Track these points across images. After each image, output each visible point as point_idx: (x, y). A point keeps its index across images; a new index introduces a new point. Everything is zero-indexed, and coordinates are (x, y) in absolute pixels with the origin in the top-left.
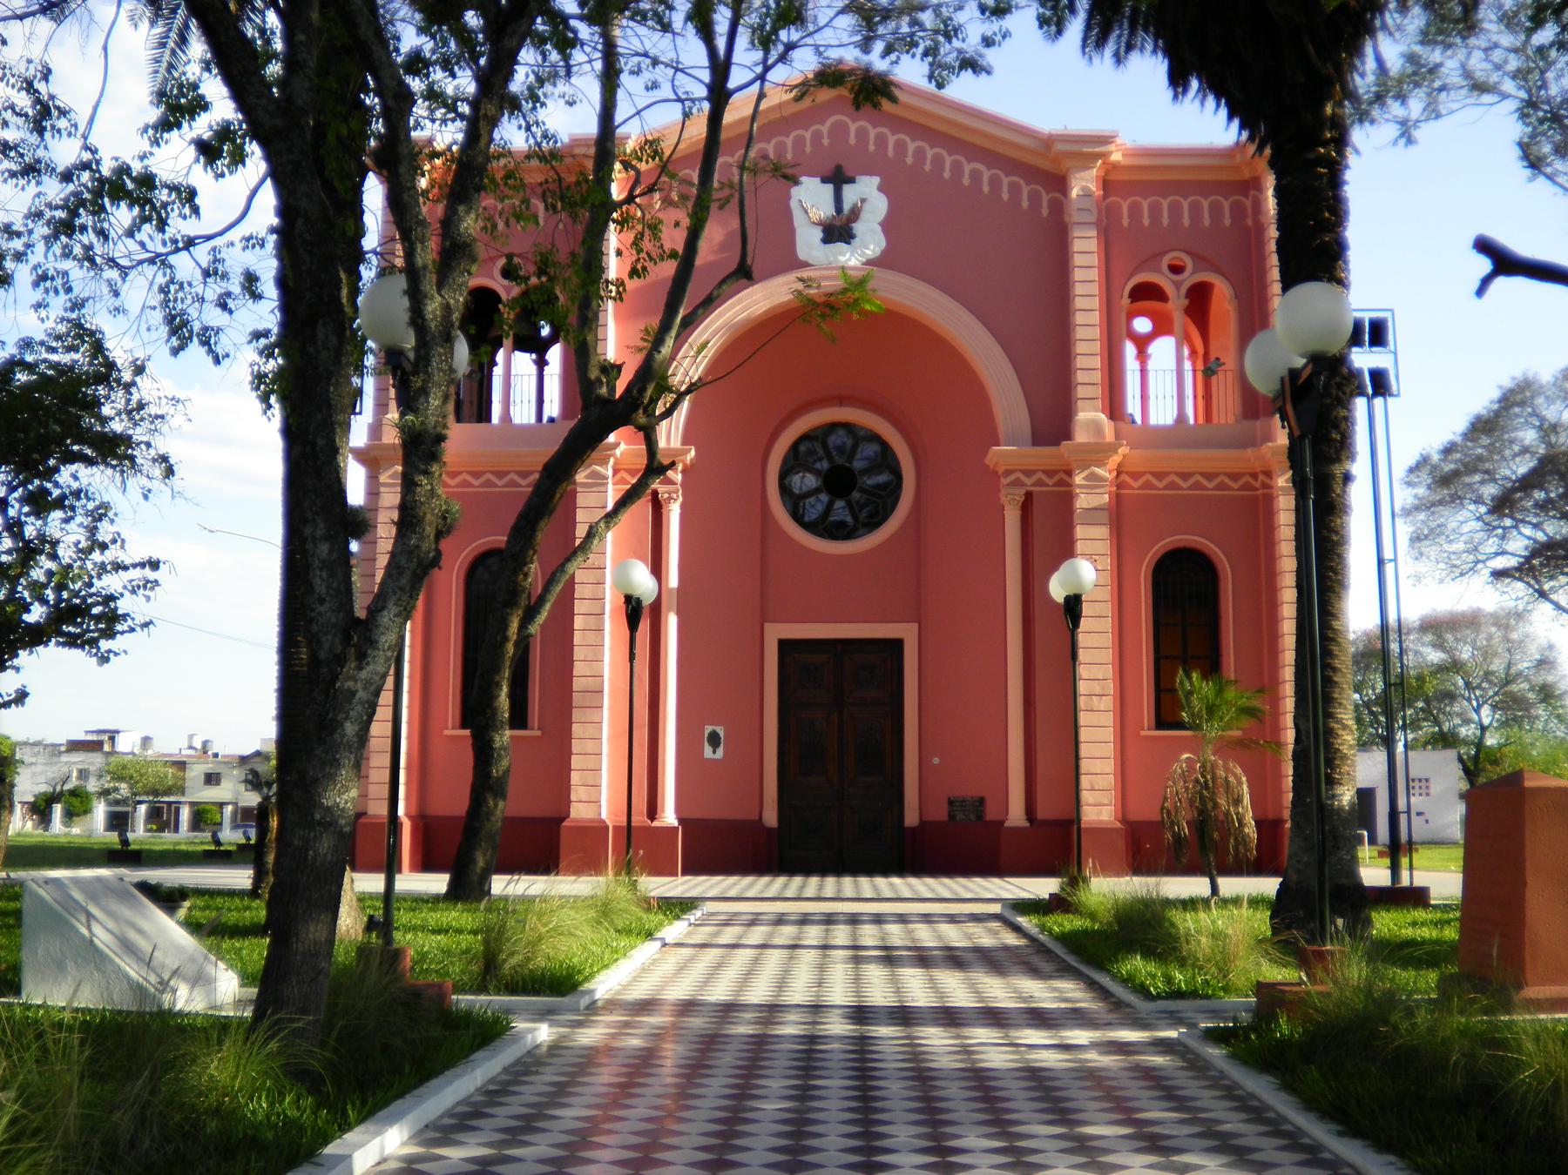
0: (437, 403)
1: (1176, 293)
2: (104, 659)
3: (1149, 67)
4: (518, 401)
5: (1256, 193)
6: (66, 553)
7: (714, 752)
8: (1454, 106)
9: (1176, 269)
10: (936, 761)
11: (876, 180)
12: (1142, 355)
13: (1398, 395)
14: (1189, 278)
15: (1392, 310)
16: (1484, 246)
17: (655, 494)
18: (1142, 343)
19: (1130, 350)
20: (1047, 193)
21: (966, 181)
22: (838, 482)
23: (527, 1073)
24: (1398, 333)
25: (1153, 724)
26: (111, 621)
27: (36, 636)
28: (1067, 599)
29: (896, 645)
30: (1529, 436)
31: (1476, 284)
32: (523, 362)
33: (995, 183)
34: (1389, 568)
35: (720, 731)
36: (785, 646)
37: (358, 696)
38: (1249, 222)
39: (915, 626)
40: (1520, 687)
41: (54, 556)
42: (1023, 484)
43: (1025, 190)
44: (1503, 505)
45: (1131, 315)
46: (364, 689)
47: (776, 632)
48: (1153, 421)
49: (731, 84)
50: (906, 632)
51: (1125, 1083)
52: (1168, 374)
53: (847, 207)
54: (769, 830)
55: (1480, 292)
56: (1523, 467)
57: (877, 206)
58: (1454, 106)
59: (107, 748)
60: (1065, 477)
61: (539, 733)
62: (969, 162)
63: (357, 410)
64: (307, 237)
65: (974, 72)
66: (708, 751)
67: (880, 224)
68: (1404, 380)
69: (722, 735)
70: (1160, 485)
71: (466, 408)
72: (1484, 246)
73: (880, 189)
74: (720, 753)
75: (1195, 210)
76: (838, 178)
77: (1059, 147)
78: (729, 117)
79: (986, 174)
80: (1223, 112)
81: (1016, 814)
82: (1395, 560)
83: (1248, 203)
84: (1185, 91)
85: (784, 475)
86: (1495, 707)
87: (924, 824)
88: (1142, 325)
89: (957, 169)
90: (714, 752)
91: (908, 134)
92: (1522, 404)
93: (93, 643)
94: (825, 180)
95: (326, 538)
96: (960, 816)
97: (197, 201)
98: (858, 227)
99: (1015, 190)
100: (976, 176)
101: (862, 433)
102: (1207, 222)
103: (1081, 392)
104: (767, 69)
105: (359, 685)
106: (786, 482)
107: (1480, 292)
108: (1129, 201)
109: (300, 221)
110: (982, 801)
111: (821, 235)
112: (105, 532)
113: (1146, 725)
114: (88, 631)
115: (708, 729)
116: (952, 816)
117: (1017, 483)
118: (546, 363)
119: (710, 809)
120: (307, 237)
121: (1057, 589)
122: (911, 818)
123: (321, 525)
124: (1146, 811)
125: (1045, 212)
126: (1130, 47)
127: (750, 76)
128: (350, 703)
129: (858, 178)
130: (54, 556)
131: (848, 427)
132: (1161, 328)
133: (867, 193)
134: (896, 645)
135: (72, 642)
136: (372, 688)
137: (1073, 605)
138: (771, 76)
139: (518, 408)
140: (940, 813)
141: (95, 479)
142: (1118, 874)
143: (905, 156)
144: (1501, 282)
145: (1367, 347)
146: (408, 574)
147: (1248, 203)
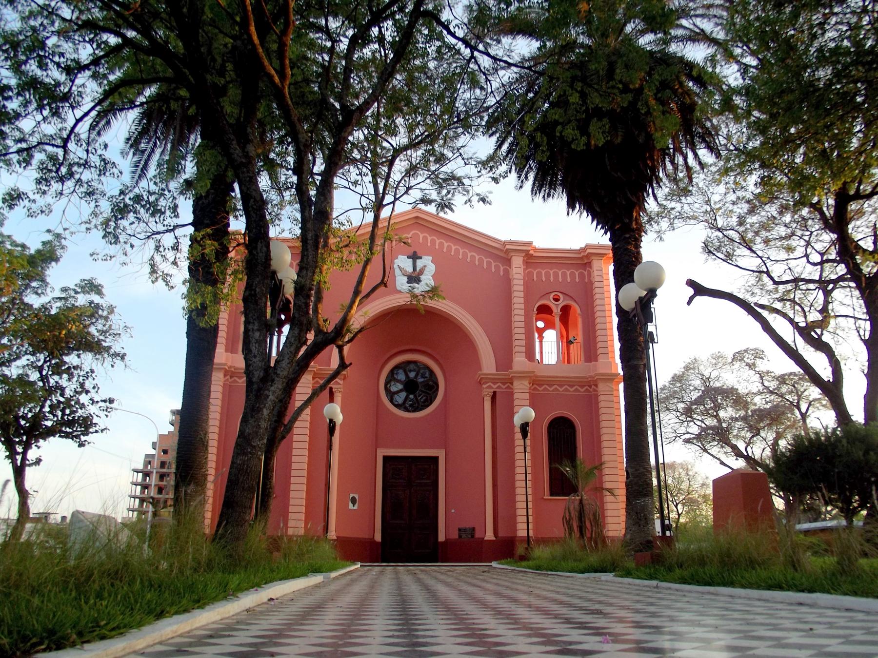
1: (557, 311)
2: (81, 445)
3: (559, 201)
6: (68, 393)
8: (680, 225)
9: (556, 299)
10: (453, 511)
11: (431, 258)
12: (541, 338)
14: (561, 303)
16: (691, 283)
17: (331, 389)
18: (541, 331)
21: (469, 260)
22: (410, 386)
23: (280, 636)
26: (87, 424)
27: (50, 432)
29: (435, 459)
30: (697, 383)
31: (687, 300)
33: (481, 260)
35: (356, 496)
36: (386, 459)
38: (586, 280)
39: (444, 452)
40: (695, 496)
41: (62, 395)
42: (492, 388)
43: (493, 264)
44: (688, 412)
47: (382, 453)
48: (545, 362)
49: (384, 203)
50: (441, 454)
53: (418, 269)
55: (689, 303)
56: (695, 395)
57: (431, 268)
58: (680, 225)
59: (44, 521)
70: (551, 389)
72: (691, 283)
73: (432, 261)
75: (564, 275)
76: (414, 257)
77: (508, 247)
79: (477, 257)
80: (590, 217)
81: (490, 535)
83: (586, 273)
84: (573, 210)
86: (684, 504)
87: (447, 541)
88: (541, 324)
89: (465, 255)
92: (694, 369)
93: (77, 437)
95: (258, 330)
96: (464, 536)
97: (179, 210)
99: (489, 263)
100: (473, 257)
102: (569, 280)
103: (517, 349)
105: (270, 393)
107: (689, 303)
110: (474, 529)
112: (88, 385)
114: (76, 431)
115: (351, 496)
116: (460, 537)
117: (490, 387)
119: (347, 534)
122: (441, 538)
125: (502, 273)
126: (549, 195)
130: (62, 395)
133: (426, 262)
134: (435, 459)
135: (67, 435)
140: (455, 535)
141: (87, 360)
144: (698, 299)
146: (294, 346)
147: (586, 273)
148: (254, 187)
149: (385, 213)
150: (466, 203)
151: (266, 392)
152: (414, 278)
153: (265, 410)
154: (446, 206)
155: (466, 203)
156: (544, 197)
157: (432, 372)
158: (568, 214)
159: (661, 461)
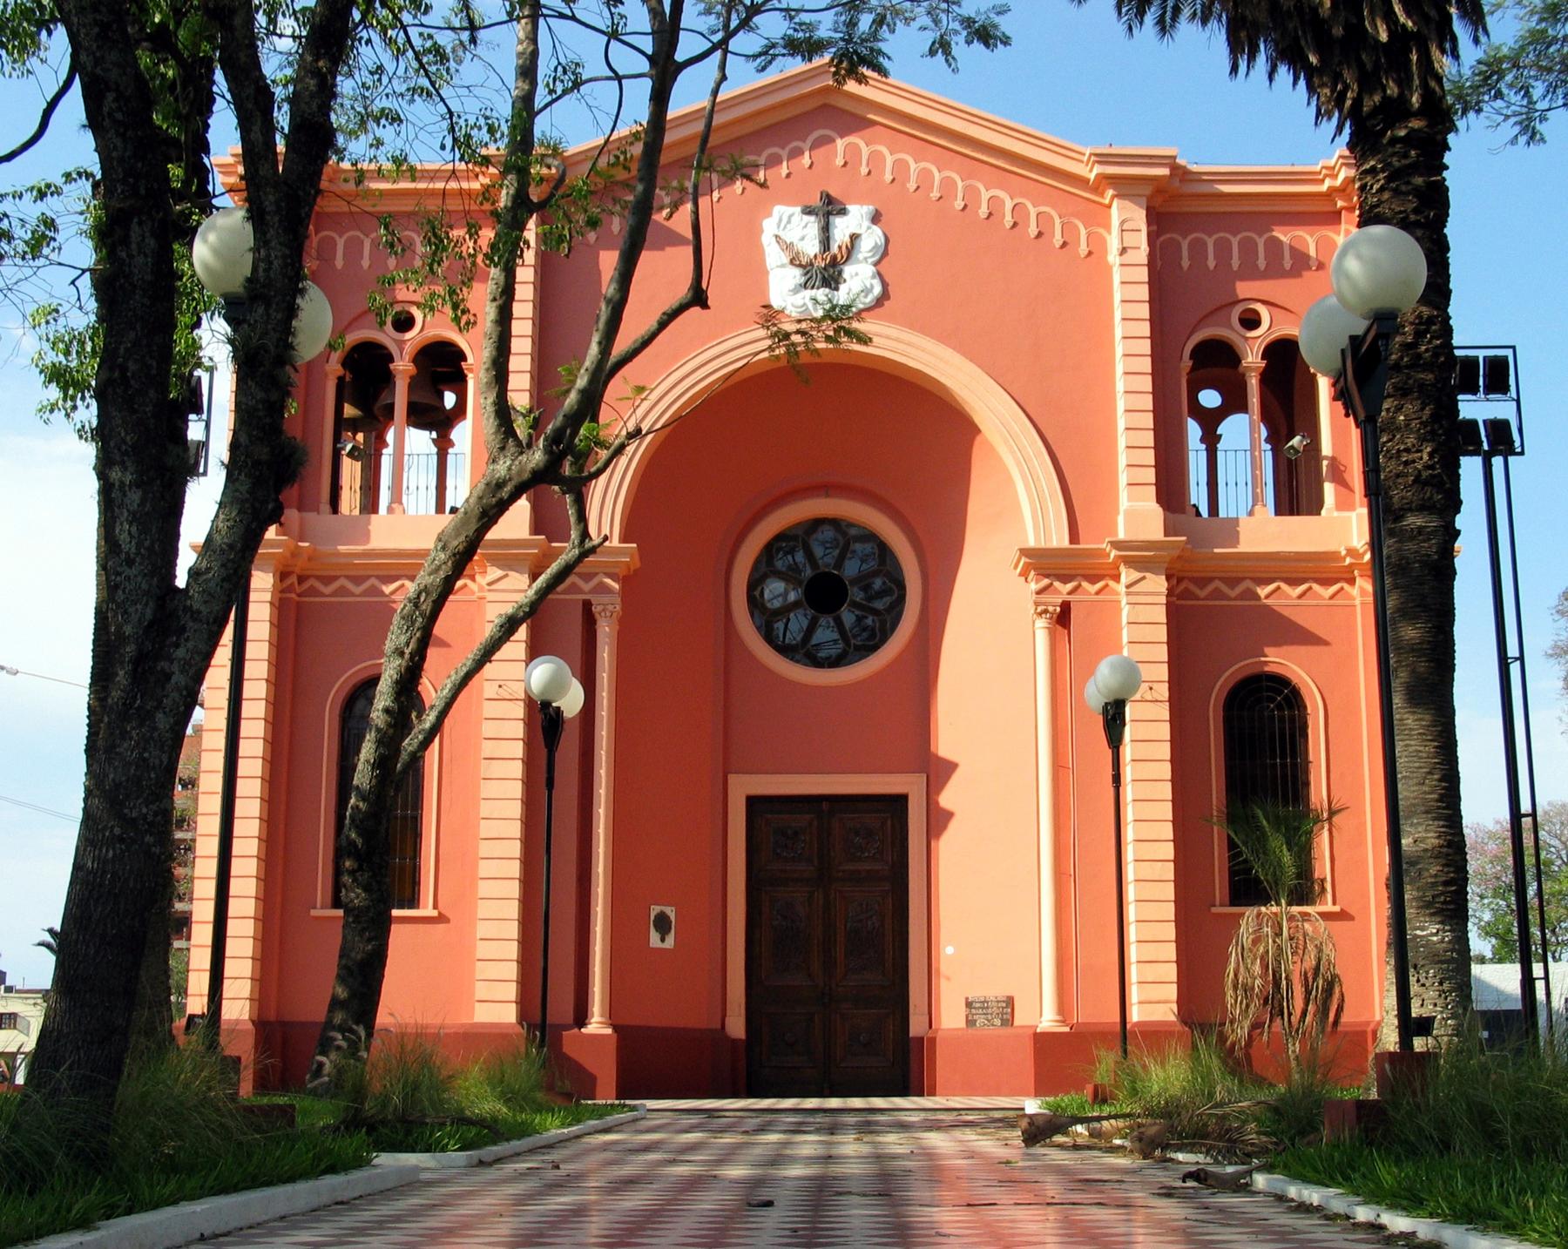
0: (279, 316)
4: (413, 487)
7: (663, 940)
12: (1211, 440)
13: (1522, 453)
15: (1514, 348)
18: (1210, 422)
19: (1194, 430)
24: (1528, 375)
25: (1227, 899)
32: (420, 441)
34: (1515, 669)
35: (671, 912)
36: (753, 803)
37: (173, 680)
46: (182, 672)
47: (743, 786)
49: (680, 56)
54: (735, 1042)
61: (435, 913)
63: (201, 470)
64: (119, 116)
65: (987, 45)
66: (654, 938)
68: (1535, 434)
69: (672, 917)
74: (670, 942)
76: (828, 209)
78: (677, 107)
82: (1521, 658)
85: (755, 584)
88: (1210, 398)
90: (663, 940)
94: (808, 211)
96: (980, 1021)
98: (848, 271)
101: (853, 532)
104: (730, 35)
105: (175, 668)
106: (757, 593)
109: (110, 96)
110: (1010, 1001)
113: (1218, 902)
115: (655, 910)
116: (970, 1022)
118: (451, 444)
120: (119, 116)
123: (131, 469)
127: (704, 45)
128: (163, 688)
132: (1235, 402)
133: (853, 222)
136: (191, 672)
138: (734, 45)
139: (413, 498)
142: (1000, 460)
145: (1481, 395)
148: (86, 79)
149: (689, 96)
150: (932, 52)
151: (163, 664)
152: (827, 273)
153: (159, 716)
154: (864, 61)
155: (932, 52)
156: (1161, 22)
157: (884, 551)
158: (1234, 69)
159: (1525, 806)
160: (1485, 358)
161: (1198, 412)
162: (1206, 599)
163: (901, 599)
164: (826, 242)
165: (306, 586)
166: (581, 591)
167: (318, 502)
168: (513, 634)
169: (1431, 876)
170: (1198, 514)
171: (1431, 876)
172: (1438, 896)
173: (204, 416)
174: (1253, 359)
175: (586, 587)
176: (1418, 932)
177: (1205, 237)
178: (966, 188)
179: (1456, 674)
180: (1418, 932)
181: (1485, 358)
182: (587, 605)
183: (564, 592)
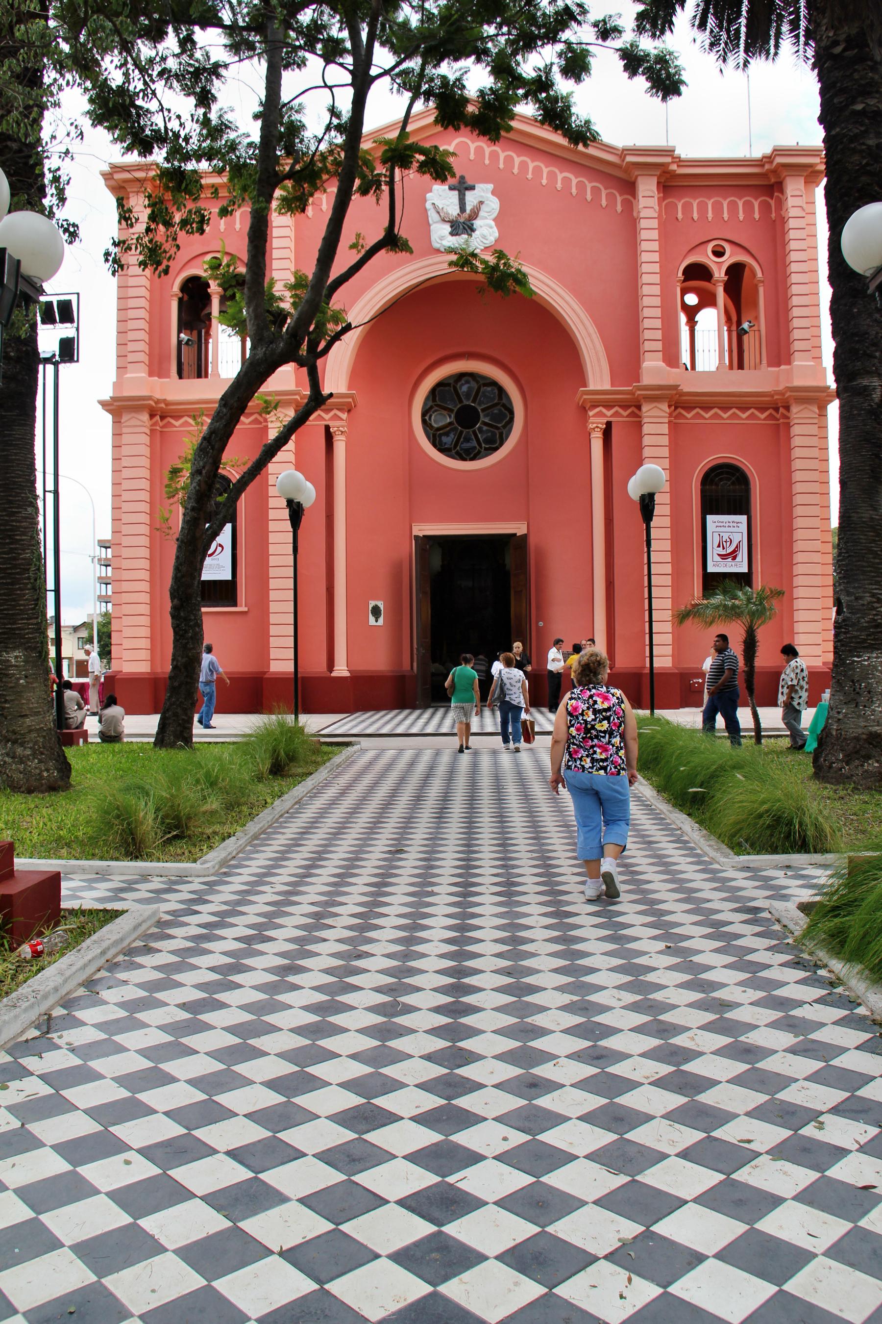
5: (780, 195)
7: (377, 621)
9: (719, 253)
11: (490, 187)
12: (692, 323)
14: (728, 259)
18: (691, 313)
19: (683, 318)
20: (620, 196)
21: (559, 186)
28: (643, 497)
35: (381, 604)
42: (605, 416)
45: (684, 292)
51: (681, 860)
52: (712, 333)
53: (468, 208)
57: (493, 205)
60: (636, 411)
61: (246, 609)
62: (561, 172)
66: (372, 620)
67: (494, 220)
69: (382, 608)
71: (185, 367)
79: (574, 181)
90: (377, 621)
91: (514, 152)
98: (477, 223)
108: (682, 201)
111: (450, 229)
115: (372, 604)
117: (600, 414)
121: (635, 487)
124: (15, 874)
129: (477, 186)
131: (472, 376)
132: (707, 300)
137: (647, 504)
143: (513, 168)
147: (772, 203)
160: (58, 302)
161: (685, 308)
162: (691, 418)
163: (512, 420)
164: (462, 208)
165: (165, 421)
166: (324, 420)
167: (169, 371)
168: (273, 456)
169: (866, 622)
170: (687, 369)
171: (866, 622)
172: (869, 635)
173: (75, 325)
174: (720, 274)
175: (327, 417)
176: (856, 659)
177: (691, 200)
178: (549, 173)
179: (259, 134)
180: (856, 659)
181: (58, 302)
182: (327, 428)
183: (313, 420)
